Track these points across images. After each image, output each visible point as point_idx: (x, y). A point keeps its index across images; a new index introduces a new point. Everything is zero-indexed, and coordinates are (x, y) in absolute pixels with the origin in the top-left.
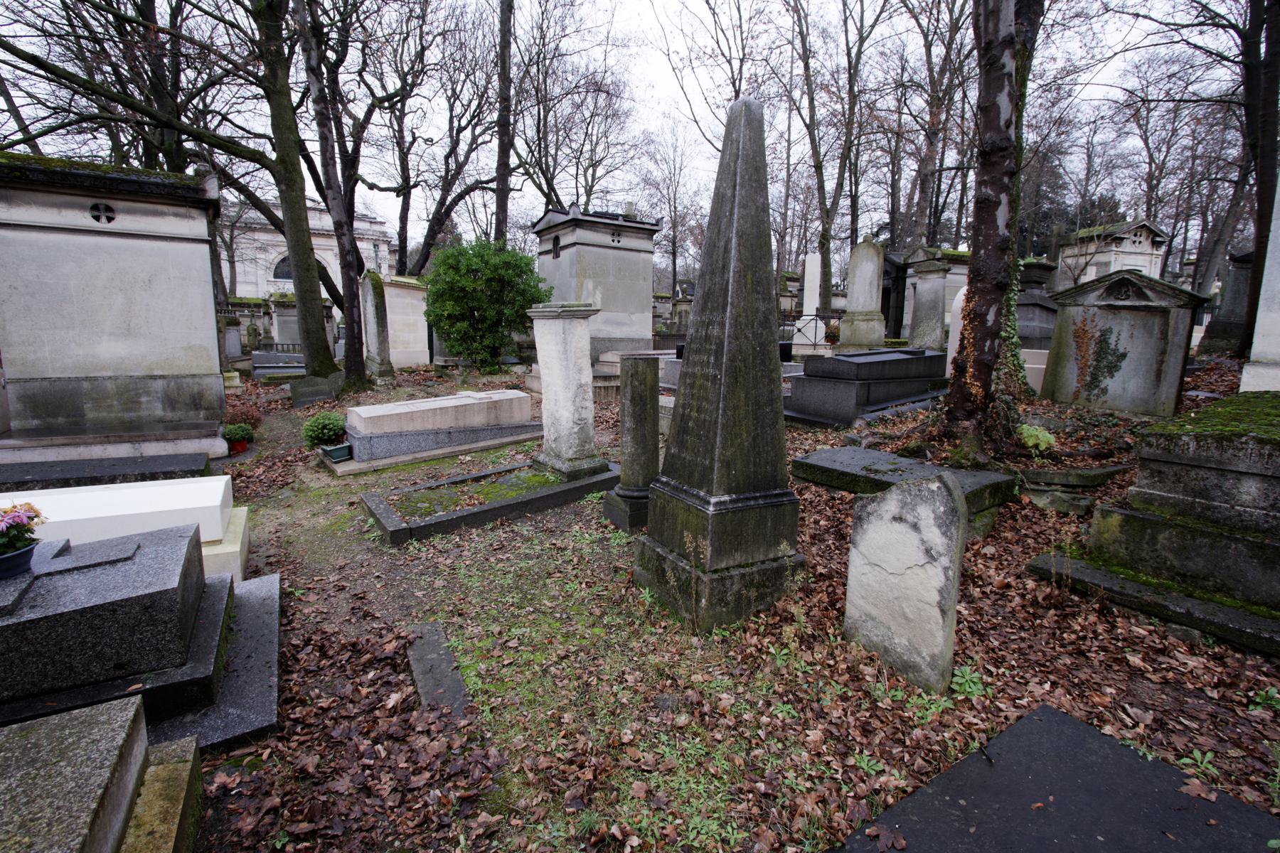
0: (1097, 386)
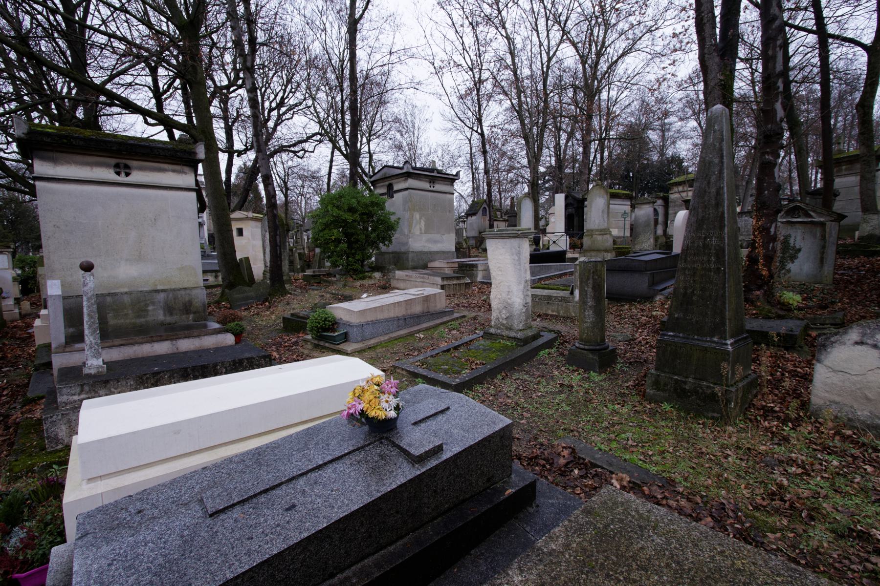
0: (784, 269)
